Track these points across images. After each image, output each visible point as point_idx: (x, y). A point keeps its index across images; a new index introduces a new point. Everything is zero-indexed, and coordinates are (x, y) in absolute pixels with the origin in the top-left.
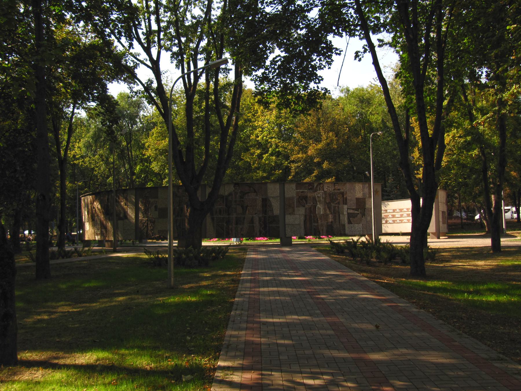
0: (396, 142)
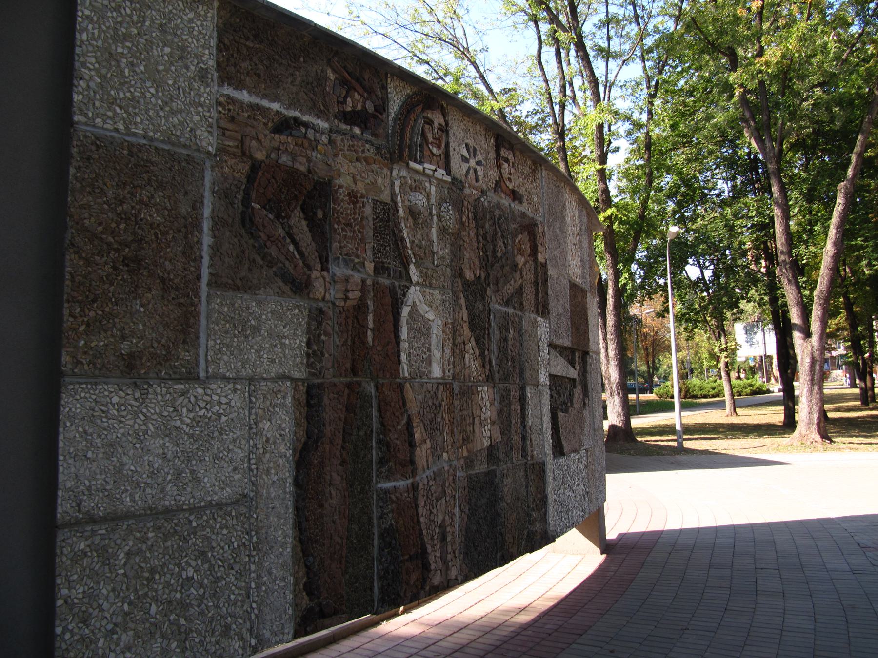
0: (58, 551)
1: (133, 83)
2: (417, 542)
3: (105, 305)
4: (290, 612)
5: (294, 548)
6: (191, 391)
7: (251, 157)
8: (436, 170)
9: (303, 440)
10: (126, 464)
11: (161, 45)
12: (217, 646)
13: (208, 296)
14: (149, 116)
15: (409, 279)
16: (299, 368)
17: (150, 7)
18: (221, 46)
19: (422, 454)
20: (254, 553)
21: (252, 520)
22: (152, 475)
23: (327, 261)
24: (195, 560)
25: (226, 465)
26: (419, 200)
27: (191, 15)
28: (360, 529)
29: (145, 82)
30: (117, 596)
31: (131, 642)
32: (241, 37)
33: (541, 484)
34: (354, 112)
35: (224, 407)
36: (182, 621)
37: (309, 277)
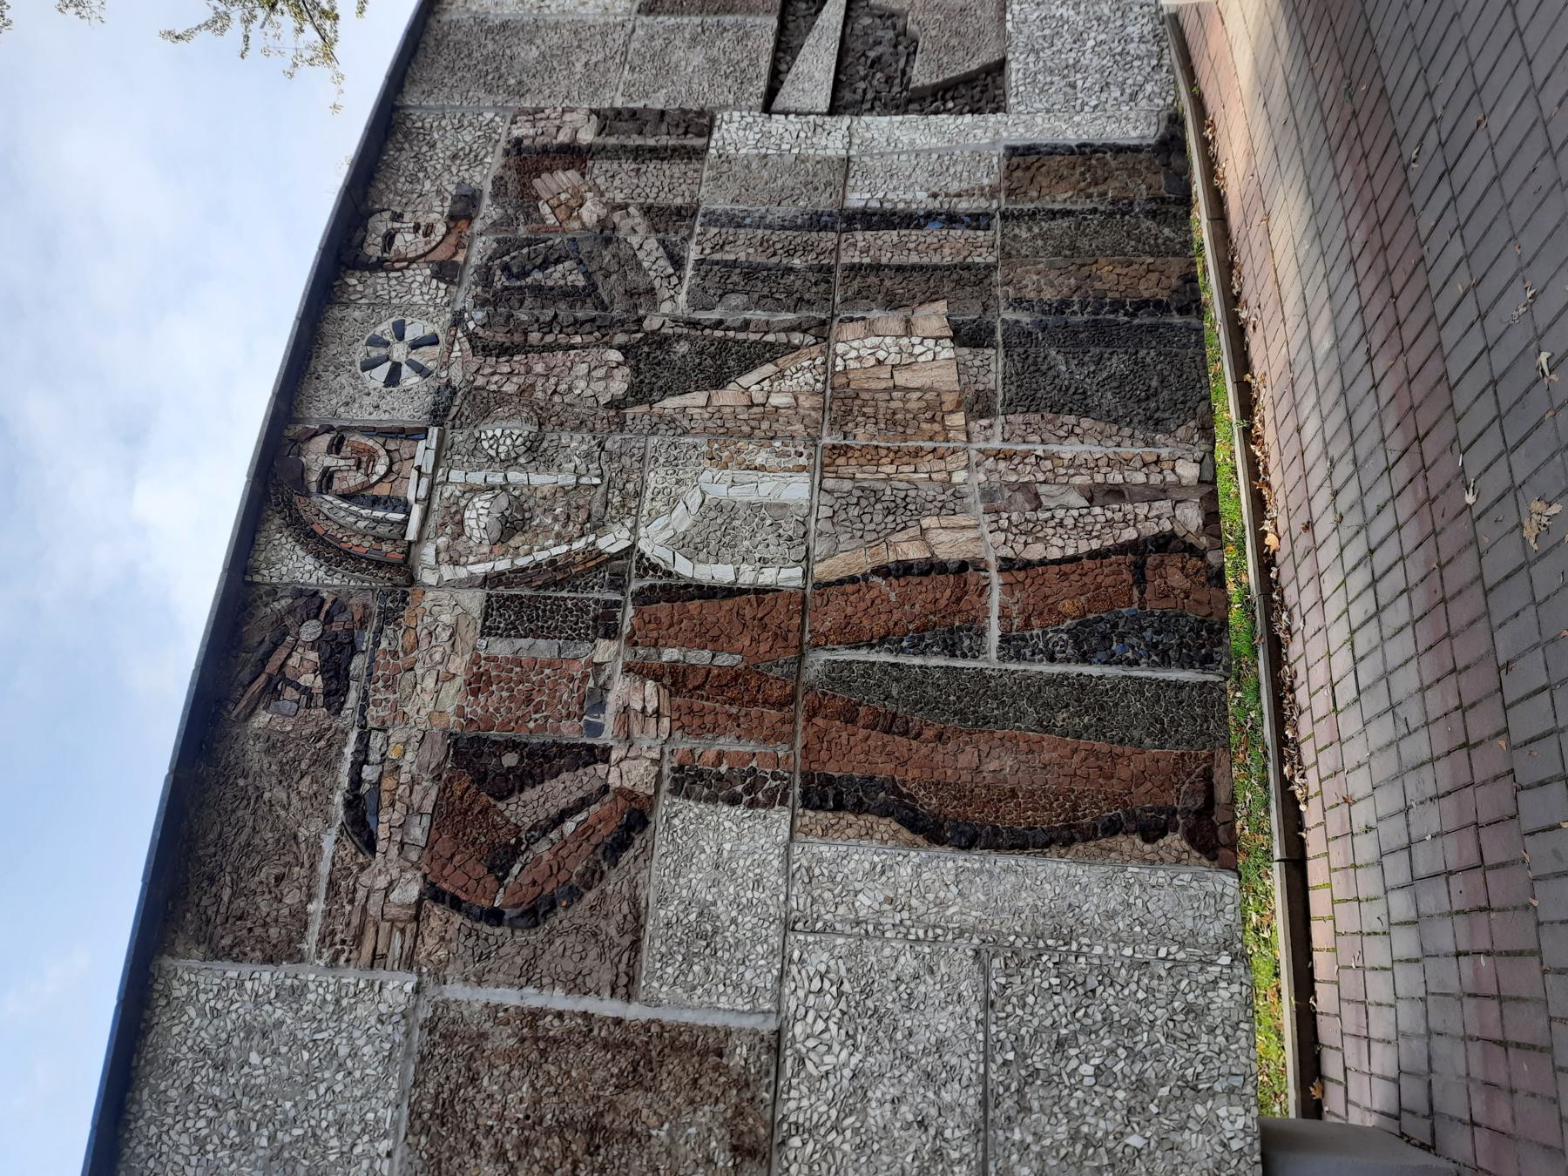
9: (895, 826)
11: (246, 1070)
12: (1218, 1032)
13: (647, 1003)
19: (949, 543)
22: (923, 1125)
24: (1069, 1059)
25: (922, 988)
27: (192, 1012)
29: (310, 1101)
35: (827, 984)
36: (1164, 1091)
37: (620, 791)
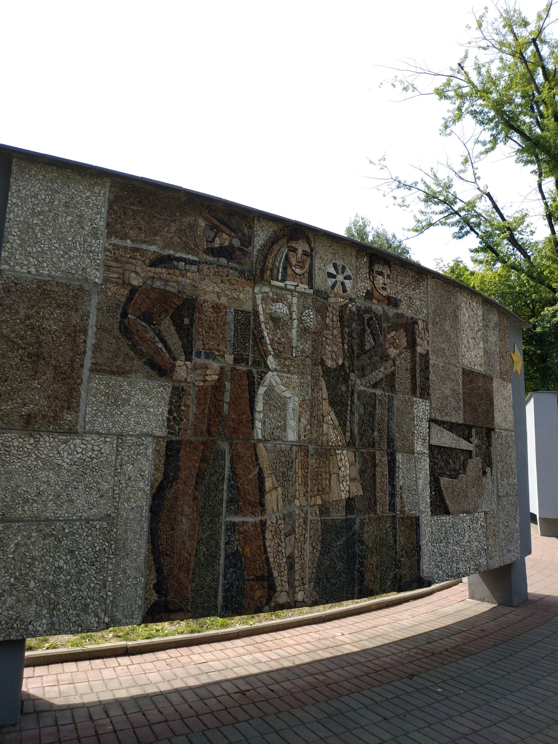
1: (43, 241)
2: (263, 567)
3: (13, 383)
4: (140, 603)
5: (146, 557)
6: (71, 441)
7: (130, 284)
8: (298, 285)
9: (160, 480)
10: (20, 486)
12: (77, 618)
13: (89, 378)
14: (53, 262)
15: (267, 367)
16: (161, 429)
17: (58, 192)
18: (111, 210)
20: (112, 556)
21: (113, 533)
23: (191, 353)
24: (66, 555)
26: (280, 308)
28: (208, 550)
29: (51, 240)
30: (7, 572)
31: (14, 604)
32: (127, 204)
33: (414, 536)
34: (221, 248)
35: (96, 453)
36: (53, 596)
37: (174, 365)
